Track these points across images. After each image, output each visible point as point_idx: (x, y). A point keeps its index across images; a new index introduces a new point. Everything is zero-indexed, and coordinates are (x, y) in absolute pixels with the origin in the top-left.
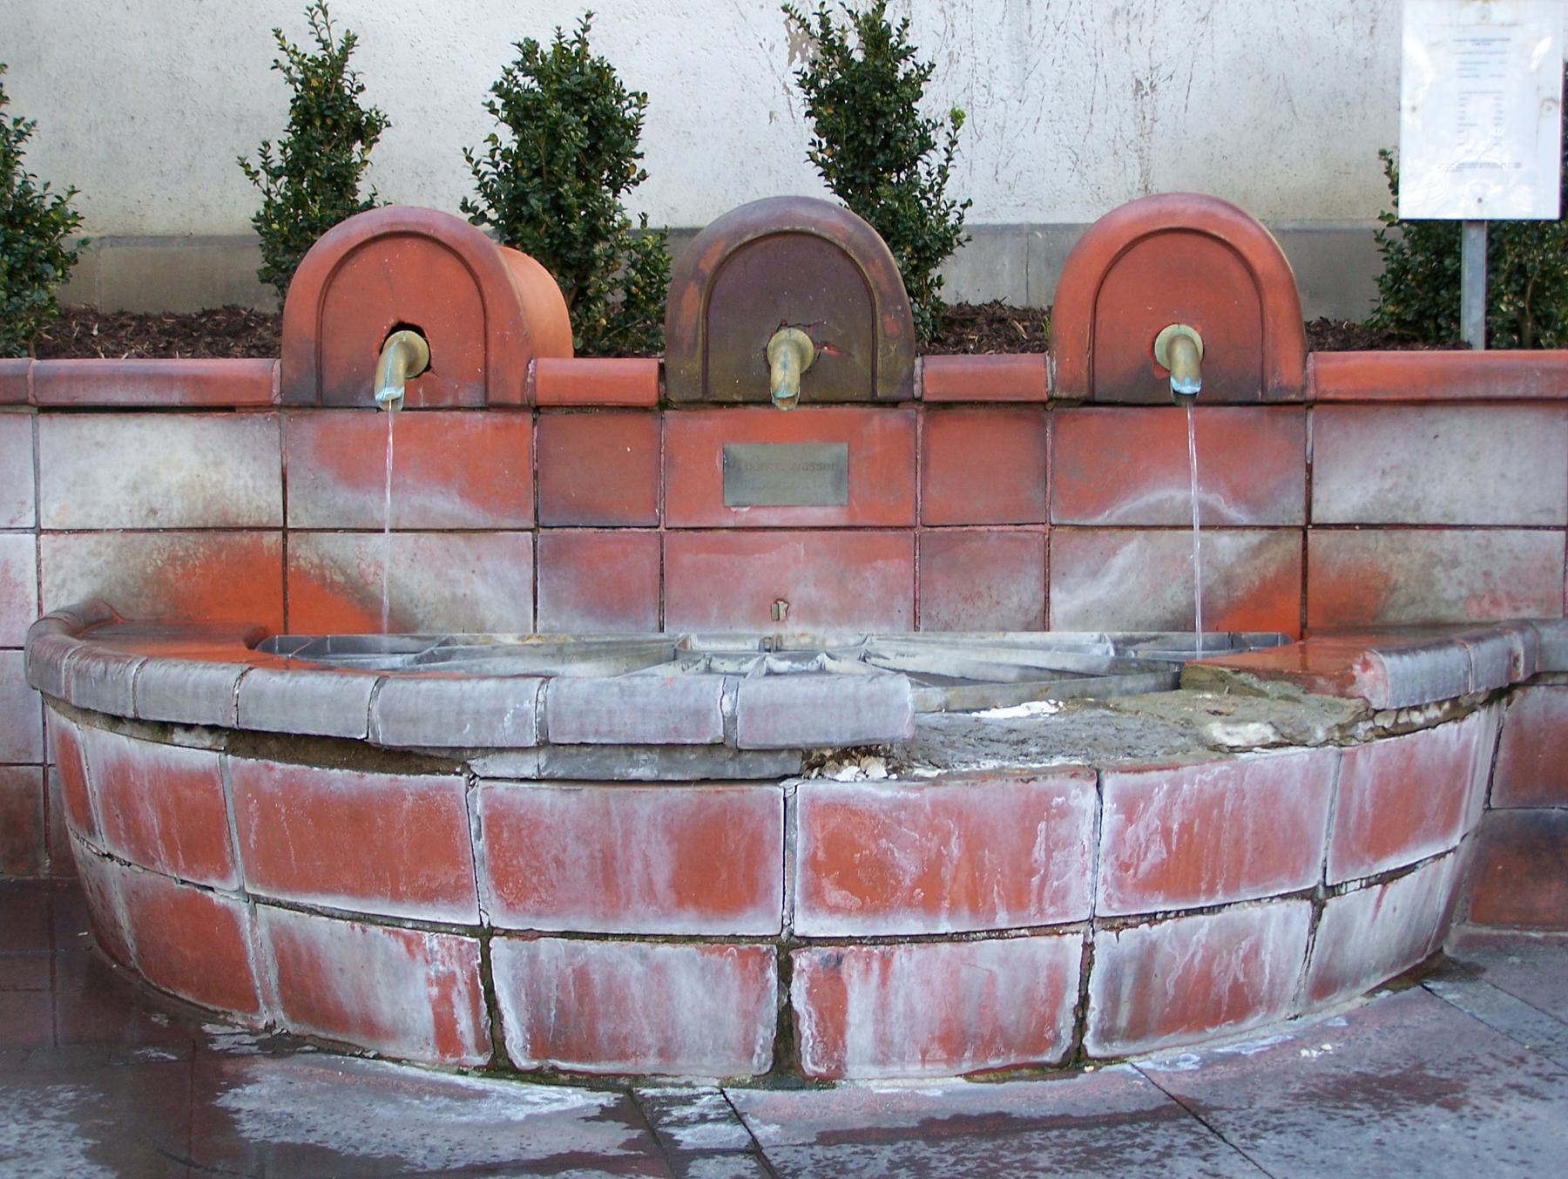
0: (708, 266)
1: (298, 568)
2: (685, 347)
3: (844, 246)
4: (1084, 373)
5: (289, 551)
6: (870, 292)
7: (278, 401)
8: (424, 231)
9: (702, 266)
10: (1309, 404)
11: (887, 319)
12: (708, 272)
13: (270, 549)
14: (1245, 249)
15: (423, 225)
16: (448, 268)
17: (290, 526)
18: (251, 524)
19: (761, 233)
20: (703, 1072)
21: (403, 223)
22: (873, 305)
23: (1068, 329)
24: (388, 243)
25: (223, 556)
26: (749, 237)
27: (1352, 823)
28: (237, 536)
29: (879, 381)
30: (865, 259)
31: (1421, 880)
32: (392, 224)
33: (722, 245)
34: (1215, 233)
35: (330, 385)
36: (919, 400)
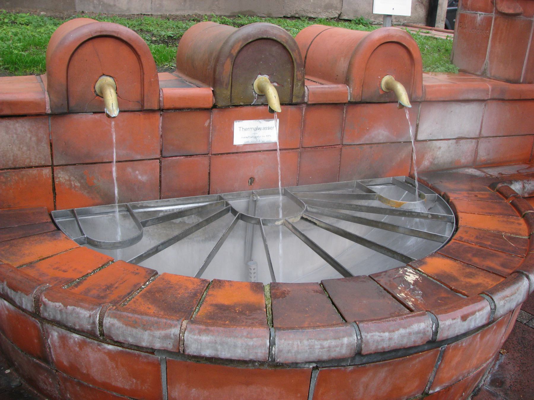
0: (235, 52)
1: (60, 182)
2: (225, 84)
3: (285, 45)
4: (361, 92)
5: (55, 175)
6: (293, 62)
7: (49, 112)
8: (116, 35)
9: (232, 52)
10: (420, 102)
11: (298, 73)
12: (234, 54)
13: (46, 175)
14: (411, 49)
15: (115, 32)
16: (125, 50)
17: (55, 164)
18: (37, 165)
19: (255, 38)
20: (414, 223)
21: (106, 31)
22: (293, 67)
23: (356, 75)
24: (99, 40)
25: (25, 179)
26: (250, 40)
27: (448, 171)
28: (31, 171)
29: (294, 97)
30: (293, 50)
31: (236, 32)
32: (101, 32)
33: (240, 43)
34: (404, 44)
35: (72, 104)
36: (306, 103)
